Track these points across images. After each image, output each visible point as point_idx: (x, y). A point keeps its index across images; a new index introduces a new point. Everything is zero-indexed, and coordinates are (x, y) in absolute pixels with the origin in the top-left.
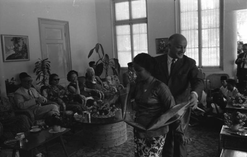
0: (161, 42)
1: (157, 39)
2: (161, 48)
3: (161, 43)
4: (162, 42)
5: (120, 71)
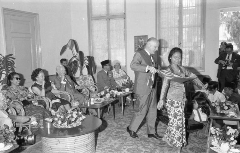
0: (140, 40)
1: (135, 37)
2: (139, 46)
3: (139, 41)
4: (141, 40)
5: (182, 31)
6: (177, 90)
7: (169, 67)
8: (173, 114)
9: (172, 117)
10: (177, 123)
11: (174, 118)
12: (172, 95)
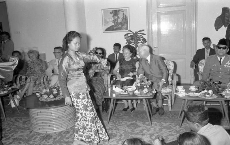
9: (83, 111)
11: (85, 111)
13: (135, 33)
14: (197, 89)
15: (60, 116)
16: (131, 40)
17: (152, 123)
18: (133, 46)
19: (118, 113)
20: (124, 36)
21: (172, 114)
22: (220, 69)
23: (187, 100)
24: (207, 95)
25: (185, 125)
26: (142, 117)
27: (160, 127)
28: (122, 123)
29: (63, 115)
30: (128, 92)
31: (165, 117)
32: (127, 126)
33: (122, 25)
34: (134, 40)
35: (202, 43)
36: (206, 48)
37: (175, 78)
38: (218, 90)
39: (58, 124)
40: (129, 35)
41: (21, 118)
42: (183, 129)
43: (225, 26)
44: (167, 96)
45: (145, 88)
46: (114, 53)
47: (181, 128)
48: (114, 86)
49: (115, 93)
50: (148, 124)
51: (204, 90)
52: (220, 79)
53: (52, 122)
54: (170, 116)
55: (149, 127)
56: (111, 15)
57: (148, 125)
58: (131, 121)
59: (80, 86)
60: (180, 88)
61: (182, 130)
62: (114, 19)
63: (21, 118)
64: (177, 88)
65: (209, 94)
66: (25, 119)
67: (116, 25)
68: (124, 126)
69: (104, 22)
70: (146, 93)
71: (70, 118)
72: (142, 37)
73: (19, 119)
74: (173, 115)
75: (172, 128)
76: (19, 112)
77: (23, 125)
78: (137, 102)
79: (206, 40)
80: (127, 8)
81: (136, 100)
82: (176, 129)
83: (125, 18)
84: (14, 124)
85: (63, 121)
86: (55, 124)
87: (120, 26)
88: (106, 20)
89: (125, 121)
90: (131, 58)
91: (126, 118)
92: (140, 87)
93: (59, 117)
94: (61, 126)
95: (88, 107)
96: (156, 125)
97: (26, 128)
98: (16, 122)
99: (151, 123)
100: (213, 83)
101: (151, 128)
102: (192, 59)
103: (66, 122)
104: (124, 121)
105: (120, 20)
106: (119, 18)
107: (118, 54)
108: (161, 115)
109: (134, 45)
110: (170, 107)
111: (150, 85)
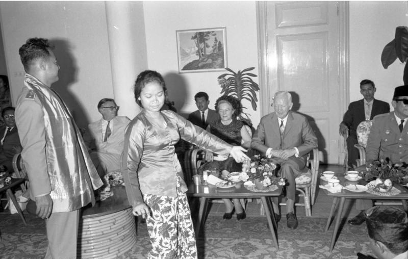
6: (162, 169)
7: (141, 119)
8: (159, 228)
9: (157, 234)
10: (169, 247)
11: (162, 236)
12: (153, 183)
13: (237, 73)
14: (361, 178)
15: (105, 232)
16: (230, 87)
17: (279, 241)
18: (235, 97)
19: (213, 221)
20: (217, 79)
21: (312, 223)
22: (400, 139)
23: (343, 199)
24: (381, 190)
25: (340, 244)
26: (258, 230)
27: (294, 250)
28: (222, 242)
29: (112, 230)
30: (232, 184)
31: (300, 230)
32: (232, 248)
33: (213, 60)
34: (236, 86)
35: (360, 90)
36: (366, 99)
37: (316, 157)
38: (402, 179)
39: (102, 247)
40: (227, 77)
41: (30, 236)
42: (338, 253)
43: (402, 61)
44: (302, 189)
45: (265, 177)
46: (198, 109)
47: (334, 251)
48: (205, 173)
49: (208, 185)
50: (271, 243)
51: (375, 179)
52: (401, 158)
53: (91, 243)
54: (311, 228)
55: (274, 249)
56: (194, 42)
57: (270, 246)
58: (238, 238)
59: (164, 181)
60: (328, 176)
61: (336, 254)
62: (199, 49)
63: (29, 234)
64: (323, 175)
65: (385, 187)
66: (37, 237)
67: (203, 59)
68: (225, 248)
69: (181, 55)
70: (268, 186)
71: (124, 236)
72: (251, 81)
73: (26, 237)
74: (315, 224)
75: (317, 251)
76: (24, 222)
77: (35, 249)
78: (247, 201)
79: (367, 85)
80: (224, 28)
81: (245, 199)
82: (325, 253)
83: (219, 47)
84: (17, 247)
85: (111, 241)
86: (95, 247)
87: (210, 61)
88: (183, 50)
89: (228, 239)
90: (231, 121)
91: (228, 231)
92: (255, 175)
93: (103, 234)
94: (107, 250)
95: (172, 228)
96: (285, 245)
97: (40, 254)
98: (19, 242)
99: (278, 243)
100: (393, 166)
101: (278, 253)
102: (342, 120)
103: (116, 242)
104: (226, 239)
105: (209, 51)
106: (208, 46)
107: (206, 112)
108: (292, 228)
109: (235, 94)
110: (308, 209)
111: (274, 170)
